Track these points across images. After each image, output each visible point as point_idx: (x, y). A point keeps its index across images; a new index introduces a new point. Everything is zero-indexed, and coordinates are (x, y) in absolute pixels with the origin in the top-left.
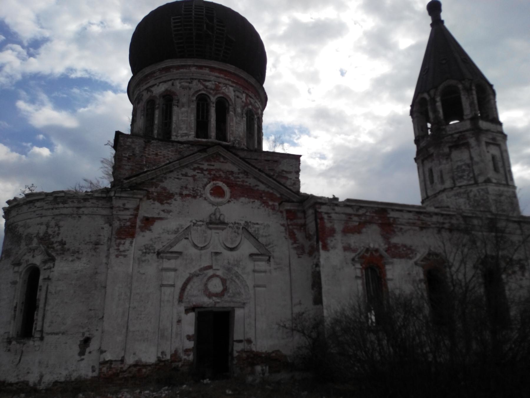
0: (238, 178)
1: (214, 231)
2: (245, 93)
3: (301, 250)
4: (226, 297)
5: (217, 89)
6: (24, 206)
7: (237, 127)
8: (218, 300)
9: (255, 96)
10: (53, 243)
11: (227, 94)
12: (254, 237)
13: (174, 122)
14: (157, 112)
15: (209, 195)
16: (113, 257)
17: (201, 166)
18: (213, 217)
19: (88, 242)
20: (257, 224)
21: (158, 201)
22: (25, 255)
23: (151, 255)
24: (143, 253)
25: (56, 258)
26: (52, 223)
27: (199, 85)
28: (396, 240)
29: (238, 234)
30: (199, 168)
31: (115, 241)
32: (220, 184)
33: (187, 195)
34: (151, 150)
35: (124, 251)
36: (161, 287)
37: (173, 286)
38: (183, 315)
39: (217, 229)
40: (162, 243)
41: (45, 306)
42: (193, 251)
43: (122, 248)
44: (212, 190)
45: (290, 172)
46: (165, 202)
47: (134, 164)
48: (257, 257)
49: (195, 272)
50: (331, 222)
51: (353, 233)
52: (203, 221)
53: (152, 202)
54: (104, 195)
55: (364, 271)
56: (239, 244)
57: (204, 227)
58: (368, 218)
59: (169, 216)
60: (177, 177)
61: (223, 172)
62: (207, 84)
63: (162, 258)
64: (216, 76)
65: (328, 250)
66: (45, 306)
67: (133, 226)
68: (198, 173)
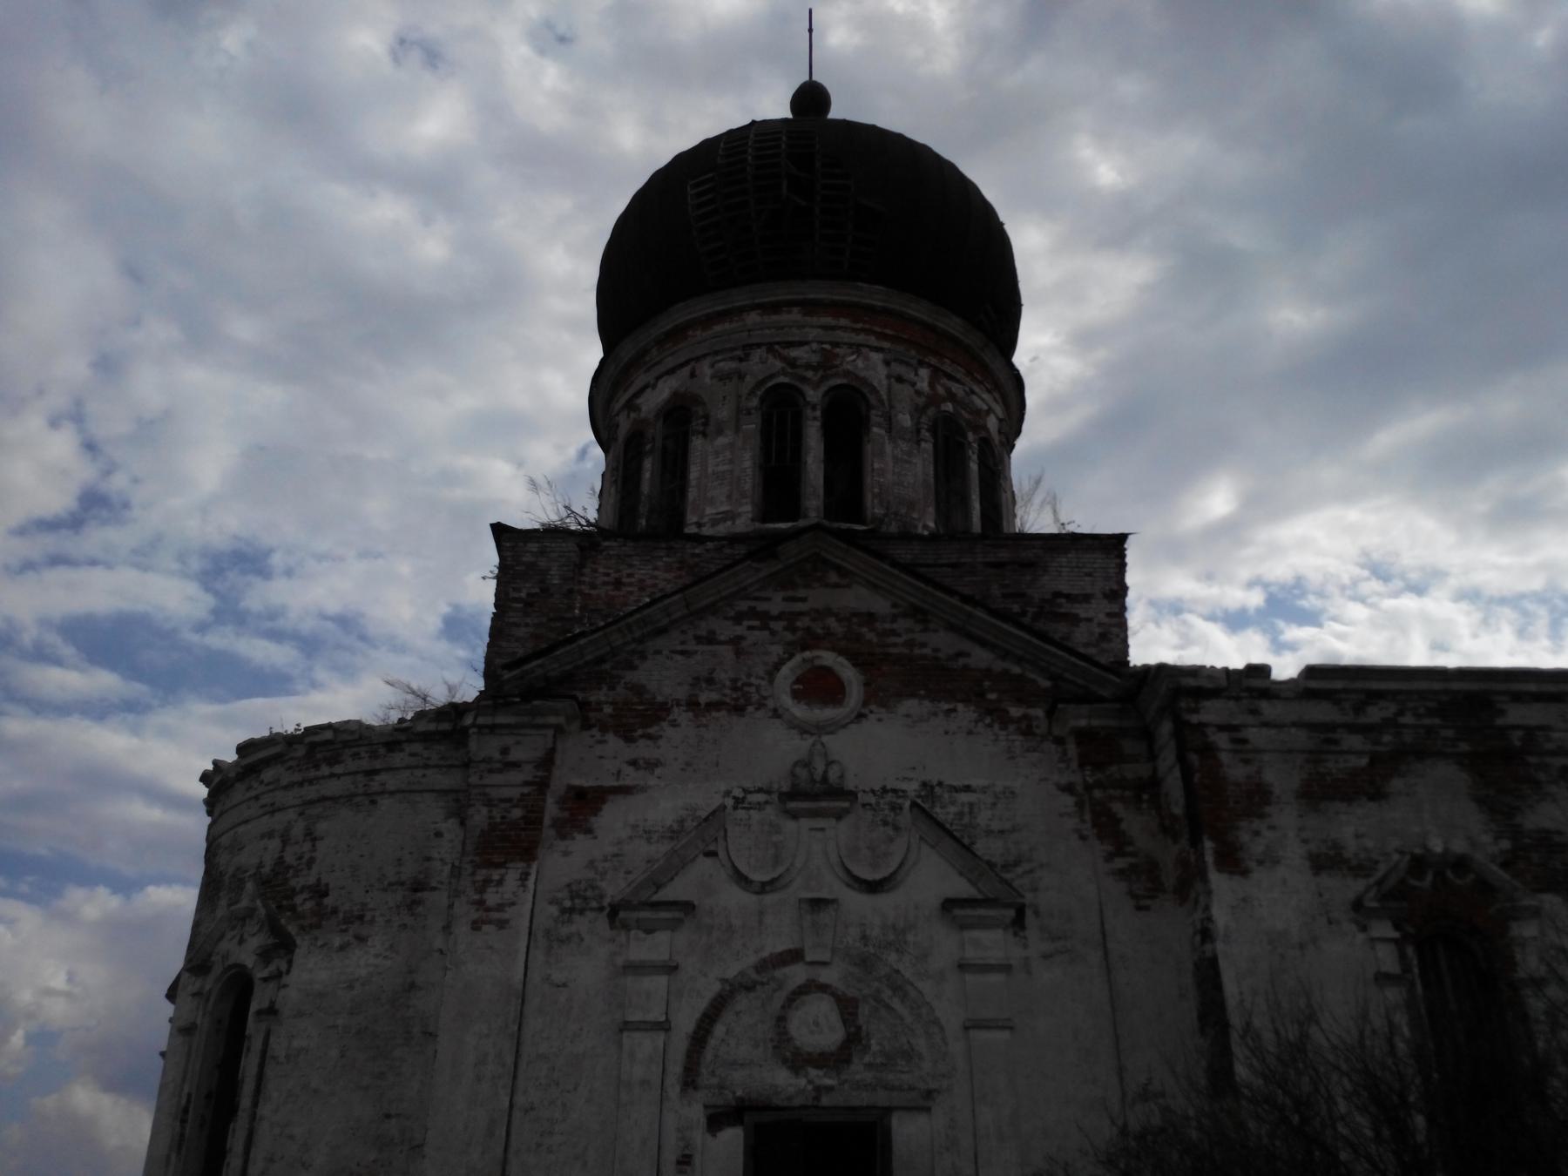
0: (894, 633)
1: (805, 823)
2: (930, 365)
3: (1144, 881)
4: (858, 1070)
5: (827, 364)
6: (238, 785)
7: (899, 472)
8: (828, 1082)
9: (969, 373)
10: (293, 892)
11: (862, 374)
12: (956, 841)
13: (693, 483)
14: (648, 464)
15: (787, 701)
16: (462, 930)
17: (762, 606)
18: (802, 773)
19: (390, 884)
20: (967, 789)
21: (616, 733)
22: (222, 937)
23: (590, 915)
24: (563, 911)
25: (298, 942)
26: (298, 830)
27: (771, 359)
28: (1543, 816)
29: (896, 828)
30: (752, 613)
31: (473, 874)
32: (828, 658)
33: (713, 706)
34: (601, 570)
35: (500, 907)
36: (621, 1031)
37: (664, 1026)
38: (699, 1136)
39: (815, 814)
40: (628, 872)
41: (255, 1104)
42: (733, 898)
43: (492, 898)
44: (798, 681)
45: (1087, 598)
46: (640, 732)
47: (544, 620)
48: (969, 912)
49: (742, 973)
50: (1247, 762)
51: (1348, 799)
52: (769, 792)
53: (598, 735)
54: (446, 726)
55: (1410, 951)
56: (901, 864)
57: (770, 812)
58: (1408, 737)
59: (652, 781)
60: (679, 648)
61: (839, 620)
62: (794, 353)
63: (626, 927)
64: (825, 328)
65: (1245, 873)
66: (255, 1104)
67: (533, 821)
68: (750, 628)
